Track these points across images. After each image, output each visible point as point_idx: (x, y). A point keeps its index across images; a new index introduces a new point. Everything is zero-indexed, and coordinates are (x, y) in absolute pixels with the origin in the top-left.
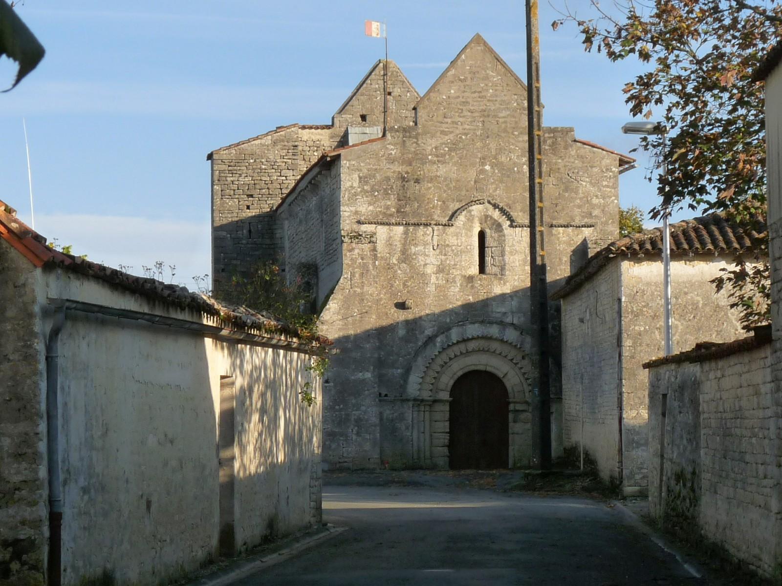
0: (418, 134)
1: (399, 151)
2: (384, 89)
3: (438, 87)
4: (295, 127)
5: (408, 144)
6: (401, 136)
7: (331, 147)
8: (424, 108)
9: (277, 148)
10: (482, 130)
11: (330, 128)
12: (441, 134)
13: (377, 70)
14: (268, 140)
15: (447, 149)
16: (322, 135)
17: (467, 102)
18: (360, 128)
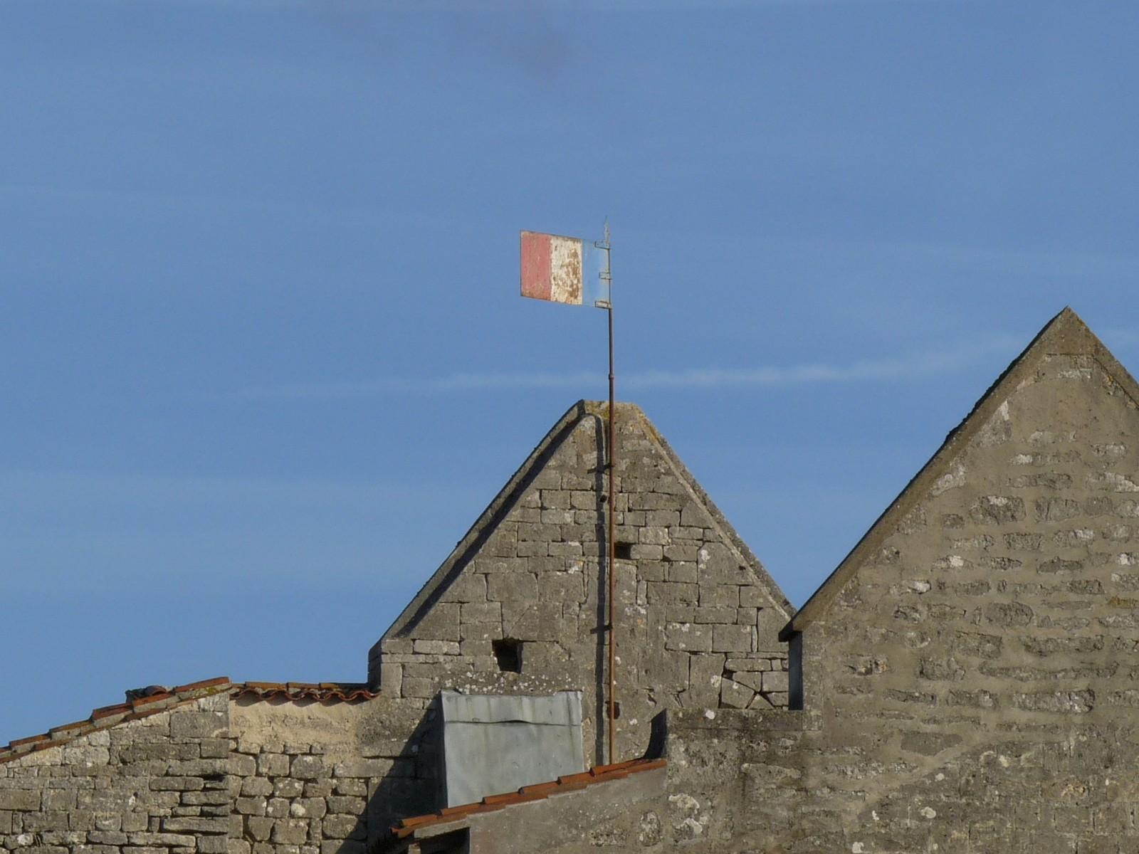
0: (805, 746)
1: (722, 819)
2: (600, 529)
3: (895, 541)
4: (212, 693)
5: (761, 787)
6: (733, 753)
7: (367, 781)
8: (831, 632)
9: (135, 783)
10: (1088, 728)
11: (361, 699)
12: (904, 746)
13: (568, 450)
14: (96, 748)
15: (931, 813)
16: (327, 726)
17: (1022, 610)
18: (494, 701)
